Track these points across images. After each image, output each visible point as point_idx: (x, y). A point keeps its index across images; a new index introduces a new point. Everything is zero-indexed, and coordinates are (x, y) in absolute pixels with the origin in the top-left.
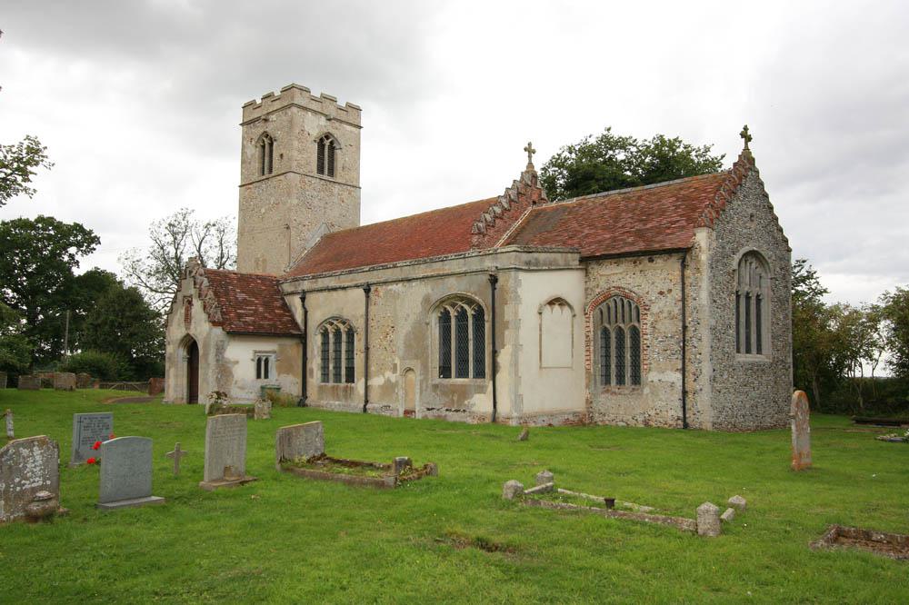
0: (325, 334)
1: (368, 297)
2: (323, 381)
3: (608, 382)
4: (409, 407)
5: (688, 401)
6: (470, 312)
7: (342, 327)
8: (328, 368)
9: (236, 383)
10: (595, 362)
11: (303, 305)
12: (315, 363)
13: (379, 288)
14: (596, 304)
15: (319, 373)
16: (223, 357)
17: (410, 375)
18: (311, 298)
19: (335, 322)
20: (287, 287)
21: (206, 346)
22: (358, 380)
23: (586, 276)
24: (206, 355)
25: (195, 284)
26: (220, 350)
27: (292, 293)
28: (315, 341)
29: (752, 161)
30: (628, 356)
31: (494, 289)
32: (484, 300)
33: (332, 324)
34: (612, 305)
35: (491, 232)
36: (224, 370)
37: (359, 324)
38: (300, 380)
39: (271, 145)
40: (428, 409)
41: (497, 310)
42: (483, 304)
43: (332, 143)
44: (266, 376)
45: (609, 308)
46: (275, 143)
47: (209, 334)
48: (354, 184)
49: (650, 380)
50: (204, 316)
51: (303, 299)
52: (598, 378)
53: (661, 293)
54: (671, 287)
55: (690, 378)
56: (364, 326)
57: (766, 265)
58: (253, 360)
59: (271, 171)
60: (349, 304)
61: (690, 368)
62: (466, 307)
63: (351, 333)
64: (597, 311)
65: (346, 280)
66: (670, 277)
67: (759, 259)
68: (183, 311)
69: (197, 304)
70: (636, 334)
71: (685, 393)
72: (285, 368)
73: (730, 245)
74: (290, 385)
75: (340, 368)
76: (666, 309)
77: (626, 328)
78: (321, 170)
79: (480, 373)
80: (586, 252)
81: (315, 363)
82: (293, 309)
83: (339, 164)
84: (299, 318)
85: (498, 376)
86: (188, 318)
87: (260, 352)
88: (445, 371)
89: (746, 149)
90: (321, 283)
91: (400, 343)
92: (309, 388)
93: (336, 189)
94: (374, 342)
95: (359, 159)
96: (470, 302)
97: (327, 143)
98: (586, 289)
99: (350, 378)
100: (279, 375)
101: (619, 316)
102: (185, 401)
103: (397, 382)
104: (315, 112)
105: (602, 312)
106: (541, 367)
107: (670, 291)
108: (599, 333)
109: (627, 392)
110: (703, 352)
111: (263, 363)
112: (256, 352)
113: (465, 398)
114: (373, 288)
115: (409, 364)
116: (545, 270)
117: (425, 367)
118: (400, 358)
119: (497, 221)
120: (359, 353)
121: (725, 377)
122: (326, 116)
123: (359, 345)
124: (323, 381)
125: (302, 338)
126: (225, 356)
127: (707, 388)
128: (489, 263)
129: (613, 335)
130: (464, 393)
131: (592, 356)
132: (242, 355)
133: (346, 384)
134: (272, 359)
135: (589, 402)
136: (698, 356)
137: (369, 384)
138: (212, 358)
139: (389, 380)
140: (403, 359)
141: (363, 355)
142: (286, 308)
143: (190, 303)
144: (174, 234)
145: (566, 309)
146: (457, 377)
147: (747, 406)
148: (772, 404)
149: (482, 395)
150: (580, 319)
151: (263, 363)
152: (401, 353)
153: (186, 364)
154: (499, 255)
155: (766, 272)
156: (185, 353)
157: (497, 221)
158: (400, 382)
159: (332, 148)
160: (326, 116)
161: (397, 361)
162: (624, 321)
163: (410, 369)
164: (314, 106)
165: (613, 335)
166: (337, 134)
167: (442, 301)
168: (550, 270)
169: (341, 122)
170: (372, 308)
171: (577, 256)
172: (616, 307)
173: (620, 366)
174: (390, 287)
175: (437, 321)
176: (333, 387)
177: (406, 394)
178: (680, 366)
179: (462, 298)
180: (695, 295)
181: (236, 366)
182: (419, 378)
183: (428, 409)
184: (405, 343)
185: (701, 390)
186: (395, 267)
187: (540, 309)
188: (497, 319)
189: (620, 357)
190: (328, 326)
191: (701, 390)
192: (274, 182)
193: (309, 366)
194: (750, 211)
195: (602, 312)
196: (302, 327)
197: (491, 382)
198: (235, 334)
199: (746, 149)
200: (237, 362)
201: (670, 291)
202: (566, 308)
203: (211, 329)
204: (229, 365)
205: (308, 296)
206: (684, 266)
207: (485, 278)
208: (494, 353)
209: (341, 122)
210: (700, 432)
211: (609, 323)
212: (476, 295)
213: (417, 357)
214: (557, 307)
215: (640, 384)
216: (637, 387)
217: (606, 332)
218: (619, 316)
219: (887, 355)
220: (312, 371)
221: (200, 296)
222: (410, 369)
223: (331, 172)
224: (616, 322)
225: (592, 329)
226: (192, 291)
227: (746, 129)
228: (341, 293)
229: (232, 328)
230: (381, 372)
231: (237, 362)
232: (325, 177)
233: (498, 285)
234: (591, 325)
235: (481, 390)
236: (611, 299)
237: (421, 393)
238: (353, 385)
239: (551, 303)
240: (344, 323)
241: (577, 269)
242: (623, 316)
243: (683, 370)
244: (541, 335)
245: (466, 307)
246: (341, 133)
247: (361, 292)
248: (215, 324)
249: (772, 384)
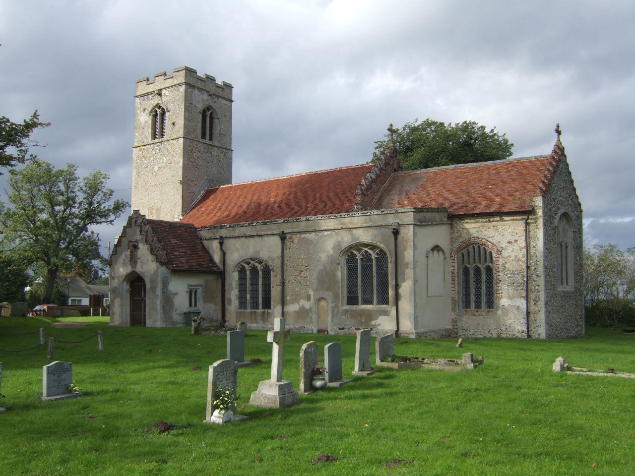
0: (242, 272)
1: (283, 243)
2: (241, 308)
3: (467, 305)
4: (322, 327)
5: (530, 319)
6: (374, 256)
7: (259, 266)
8: (246, 298)
9: (176, 311)
10: (458, 292)
11: (221, 248)
12: (233, 294)
13: (294, 236)
14: (459, 249)
15: (237, 302)
16: (167, 289)
17: (323, 303)
18: (229, 243)
19: (253, 262)
20: (204, 234)
21: (152, 281)
22: (274, 308)
23: (451, 229)
24: (153, 288)
25: (141, 231)
26: (165, 284)
27: (211, 239)
28: (233, 278)
29: (562, 150)
30: (484, 287)
31: (396, 239)
32: (387, 246)
33: (248, 263)
34: (471, 250)
35: (369, 193)
36: (168, 300)
37: (276, 264)
38: (219, 307)
39: (163, 114)
40: (340, 329)
41: (398, 255)
42: (385, 249)
43: (211, 114)
44: (196, 305)
45: (469, 253)
46: (167, 114)
47: (156, 272)
48: (228, 147)
49: (501, 304)
50: (150, 257)
51: (221, 244)
52: (461, 304)
53: (509, 242)
54: (517, 238)
55: (532, 303)
56: (280, 265)
57: (571, 222)
58: (187, 292)
59: (162, 135)
60: (267, 248)
61: (532, 296)
62: (370, 251)
63: (267, 271)
64: (460, 255)
65: (263, 230)
66: (517, 231)
67: (566, 217)
68: (128, 253)
69: (143, 249)
70: (489, 270)
71: (528, 313)
72: (208, 298)
73: (553, 209)
74: (209, 310)
75: (258, 298)
76: (513, 255)
77: (482, 267)
78: (203, 137)
79: (384, 300)
80: (452, 213)
81: (233, 294)
82: (211, 251)
83: (216, 132)
84: (217, 258)
85: (400, 303)
86: (133, 260)
87: (191, 286)
88: (352, 300)
89: (559, 140)
90: (238, 231)
91: (314, 279)
92: (227, 314)
93: (215, 152)
94: (290, 278)
95: (231, 126)
96: (373, 247)
97: (208, 113)
98: (452, 238)
99: (267, 304)
100: (204, 304)
101: (477, 258)
102: (129, 325)
103: (311, 309)
104: (200, 89)
105: (463, 255)
106: (428, 297)
107: (516, 241)
108: (461, 271)
109: (484, 313)
110: (540, 284)
111: (193, 294)
112: (189, 286)
113: (372, 319)
114: (288, 236)
115: (321, 294)
116: (430, 225)
117: (336, 296)
118: (313, 290)
119: (373, 184)
120: (275, 286)
121: (552, 301)
122: (208, 92)
123: (275, 280)
124: (241, 308)
125: (221, 275)
126: (169, 289)
127: (543, 310)
128: (391, 220)
129: (472, 273)
130: (370, 316)
131: (456, 287)
132: (180, 287)
133: (263, 310)
134: (200, 291)
135: (454, 322)
136: (537, 287)
137: (285, 310)
138: (159, 291)
139: (303, 307)
140: (315, 291)
141: (279, 288)
142: (206, 252)
143: (136, 247)
144: (44, 183)
145: (441, 253)
146: (378, 303)
147: (563, 322)
148: (574, 321)
149: (386, 317)
150: (449, 260)
151: (193, 294)
152: (315, 286)
153: (129, 295)
154: (399, 214)
155: (570, 228)
156: (128, 287)
157: (373, 184)
158: (314, 309)
159: (212, 118)
160: (208, 92)
161: (311, 292)
162: (480, 262)
163: (323, 298)
164: (199, 84)
165: (472, 273)
166: (215, 106)
167: (350, 247)
168: (433, 225)
169: (218, 97)
170: (287, 252)
171: (446, 214)
172: (474, 252)
173: (478, 295)
174: (303, 236)
175: (345, 262)
176: (251, 313)
177: (319, 317)
178: (524, 294)
179: (366, 245)
180: (534, 244)
181: (176, 296)
182: (331, 305)
183: (340, 329)
184: (317, 279)
185: (539, 311)
186: (308, 220)
187: (427, 254)
188: (399, 261)
189: (478, 288)
190: (245, 265)
191: (539, 311)
192: (166, 145)
193: (227, 296)
194: (563, 184)
195: (463, 255)
196: (221, 267)
197: (395, 308)
198: (177, 272)
199: (559, 140)
200: (176, 294)
201: (516, 241)
202: (441, 253)
203: (158, 268)
204: (172, 296)
205: (225, 241)
206: (527, 224)
207: (389, 232)
208: (397, 286)
209: (218, 97)
210: (538, 341)
211: (469, 263)
212: (380, 243)
213: (328, 289)
214: (436, 252)
215: (493, 308)
216: (491, 310)
217: (466, 271)
218: (477, 258)
219: (42, 279)
220: (230, 300)
221: (147, 241)
222: (323, 298)
223: (211, 139)
224: (463, 263)
225: (456, 268)
226: (138, 237)
227: (558, 126)
228: (257, 239)
229: (174, 267)
230: (295, 301)
231: (176, 294)
232: (207, 141)
233: (400, 237)
234: (456, 265)
235: (386, 313)
236: (471, 246)
237: (333, 317)
238: (269, 311)
239: (433, 250)
240: (260, 263)
241: (446, 224)
242: (480, 259)
243: (527, 298)
244: (427, 272)
245: (370, 251)
246: (218, 105)
247: (277, 240)
248: (162, 264)
249: (574, 306)
